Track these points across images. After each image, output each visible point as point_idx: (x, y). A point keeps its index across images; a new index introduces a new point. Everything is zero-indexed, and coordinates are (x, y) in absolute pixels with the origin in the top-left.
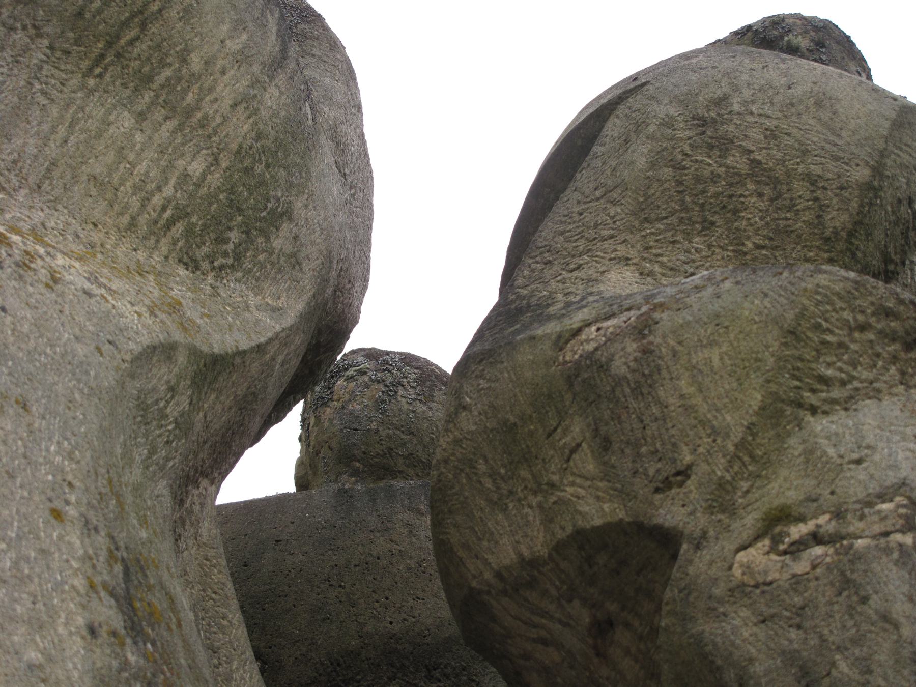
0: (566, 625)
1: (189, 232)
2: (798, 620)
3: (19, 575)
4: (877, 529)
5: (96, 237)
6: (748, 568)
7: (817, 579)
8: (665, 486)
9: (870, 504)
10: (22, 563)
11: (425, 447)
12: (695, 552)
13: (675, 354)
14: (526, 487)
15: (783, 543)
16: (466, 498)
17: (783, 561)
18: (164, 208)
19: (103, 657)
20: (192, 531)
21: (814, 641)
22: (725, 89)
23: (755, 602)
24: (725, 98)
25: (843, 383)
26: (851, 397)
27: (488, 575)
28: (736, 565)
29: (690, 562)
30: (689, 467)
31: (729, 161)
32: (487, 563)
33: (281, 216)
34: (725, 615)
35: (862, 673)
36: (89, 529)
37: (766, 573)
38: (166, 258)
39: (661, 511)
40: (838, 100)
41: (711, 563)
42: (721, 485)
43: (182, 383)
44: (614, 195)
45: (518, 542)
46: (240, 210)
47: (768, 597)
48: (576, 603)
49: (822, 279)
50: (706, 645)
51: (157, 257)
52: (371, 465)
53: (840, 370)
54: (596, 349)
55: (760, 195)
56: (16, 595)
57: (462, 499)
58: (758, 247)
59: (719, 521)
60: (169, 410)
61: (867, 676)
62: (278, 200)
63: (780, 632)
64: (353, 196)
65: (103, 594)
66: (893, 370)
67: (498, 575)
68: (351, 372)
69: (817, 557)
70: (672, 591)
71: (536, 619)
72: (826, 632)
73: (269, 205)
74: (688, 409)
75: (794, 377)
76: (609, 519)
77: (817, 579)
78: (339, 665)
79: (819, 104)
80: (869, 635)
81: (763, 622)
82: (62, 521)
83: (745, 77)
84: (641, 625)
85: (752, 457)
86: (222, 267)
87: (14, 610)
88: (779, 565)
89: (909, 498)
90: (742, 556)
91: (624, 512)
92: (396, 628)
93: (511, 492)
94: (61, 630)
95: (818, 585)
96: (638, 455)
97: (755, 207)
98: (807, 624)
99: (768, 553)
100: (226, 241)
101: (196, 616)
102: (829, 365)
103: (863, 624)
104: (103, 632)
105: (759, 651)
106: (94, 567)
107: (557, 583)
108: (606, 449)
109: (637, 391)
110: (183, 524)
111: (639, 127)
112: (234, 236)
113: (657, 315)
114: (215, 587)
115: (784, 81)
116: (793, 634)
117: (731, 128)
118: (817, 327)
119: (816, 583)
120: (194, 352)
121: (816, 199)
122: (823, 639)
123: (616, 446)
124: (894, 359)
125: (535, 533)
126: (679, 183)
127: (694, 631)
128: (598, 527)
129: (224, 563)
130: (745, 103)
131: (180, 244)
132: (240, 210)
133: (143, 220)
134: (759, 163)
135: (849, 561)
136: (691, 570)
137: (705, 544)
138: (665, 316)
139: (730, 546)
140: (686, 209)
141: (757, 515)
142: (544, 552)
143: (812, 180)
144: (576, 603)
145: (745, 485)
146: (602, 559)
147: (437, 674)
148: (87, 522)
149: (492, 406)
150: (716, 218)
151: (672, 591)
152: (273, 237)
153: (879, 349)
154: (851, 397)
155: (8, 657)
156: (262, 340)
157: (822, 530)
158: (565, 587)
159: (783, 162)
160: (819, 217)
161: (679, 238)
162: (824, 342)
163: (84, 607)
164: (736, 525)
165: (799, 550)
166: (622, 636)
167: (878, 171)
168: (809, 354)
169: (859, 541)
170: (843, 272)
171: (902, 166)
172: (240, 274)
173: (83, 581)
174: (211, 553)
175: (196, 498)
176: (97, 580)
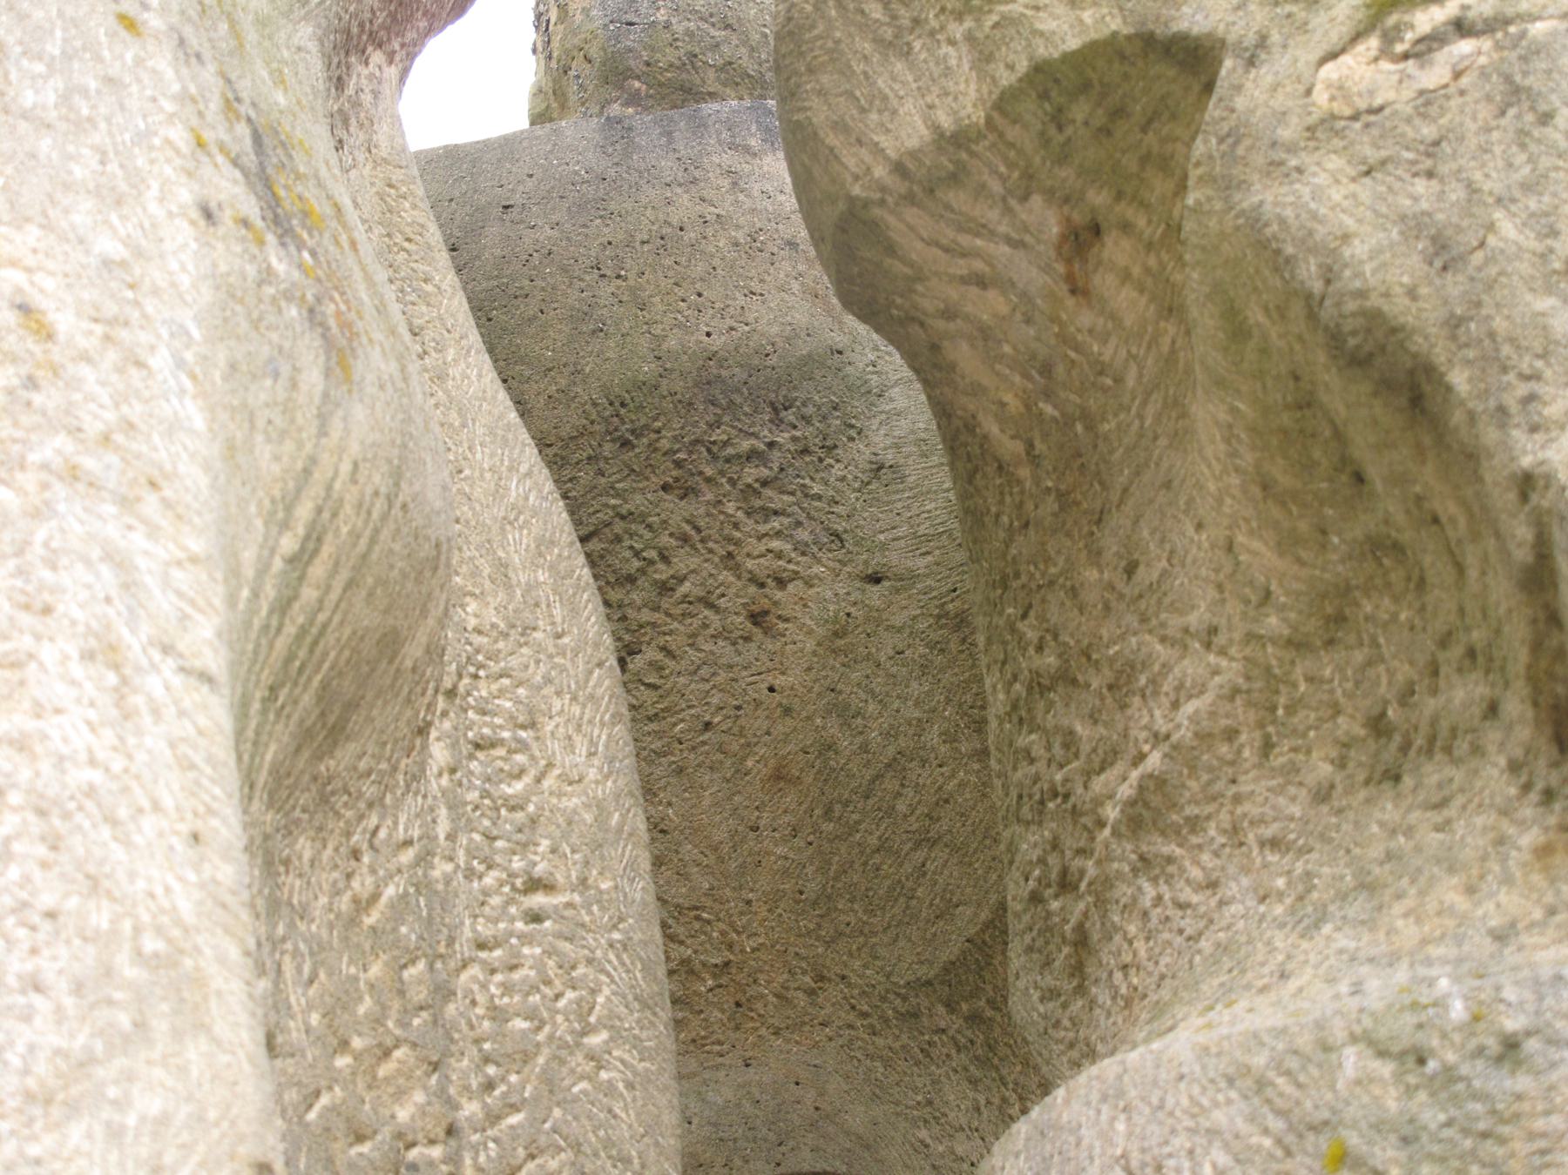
2: (1429, 163)
3: (72, 116)
6: (1340, 90)
7: (1462, 93)
10: (77, 100)
11: (753, 49)
12: (1247, 72)
14: (943, 9)
15: (1402, 40)
16: (838, 42)
17: (1402, 71)
19: (228, 254)
20: (362, 136)
21: (1456, 193)
23: (1352, 143)
27: (880, 171)
28: (1319, 87)
29: (1238, 88)
32: (878, 150)
34: (1299, 170)
35: (1541, 237)
36: (185, 52)
37: (1371, 93)
39: (1185, 9)
41: (1274, 88)
45: (931, 107)
47: (1375, 132)
48: (1037, 201)
50: (1266, 225)
52: (661, 85)
56: (71, 148)
57: (830, 44)
59: (1289, 16)
61: (1549, 242)
63: (1397, 185)
65: (220, 159)
67: (899, 169)
69: (1463, 58)
70: (1206, 142)
71: (965, 240)
72: (1478, 176)
76: (1094, 35)
77: (1462, 93)
78: (623, 405)
80: (1553, 174)
81: (1368, 173)
82: (139, 34)
84: (1150, 222)
87: (70, 173)
88: (1396, 77)
90: (1330, 71)
91: (1119, 20)
92: (717, 342)
94: (153, 207)
95: (1465, 104)
98: (1444, 169)
99: (1376, 59)
103: (1543, 158)
104: (227, 217)
105: (1360, 221)
106: (200, 114)
107: (1002, 169)
110: (346, 122)
114: (408, 230)
116: (1420, 186)
119: (1460, 100)
122: (1472, 189)
125: (962, 87)
127: (1245, 205)
128: (1074, 53)
129: (420, 192)
135: (1521, 58)
136: (1240, 103)
137: (1263, 56)
142: (979, 116)
144: (1037, 201)
146: (1079, 111)
147: (789, 416)
148: (182, 42)
151: (1206, 142)
155: (67, 247)
157: (1471, 14)
158: (1016, 174)
163: (190, 174)
164: (1319, 20)
165: (1430, 50)
166: (1116, 249)
169: (1539, 25)
173: (185, 135)
174: (397, 176)
175: (364, 81)
176: (208, 136)
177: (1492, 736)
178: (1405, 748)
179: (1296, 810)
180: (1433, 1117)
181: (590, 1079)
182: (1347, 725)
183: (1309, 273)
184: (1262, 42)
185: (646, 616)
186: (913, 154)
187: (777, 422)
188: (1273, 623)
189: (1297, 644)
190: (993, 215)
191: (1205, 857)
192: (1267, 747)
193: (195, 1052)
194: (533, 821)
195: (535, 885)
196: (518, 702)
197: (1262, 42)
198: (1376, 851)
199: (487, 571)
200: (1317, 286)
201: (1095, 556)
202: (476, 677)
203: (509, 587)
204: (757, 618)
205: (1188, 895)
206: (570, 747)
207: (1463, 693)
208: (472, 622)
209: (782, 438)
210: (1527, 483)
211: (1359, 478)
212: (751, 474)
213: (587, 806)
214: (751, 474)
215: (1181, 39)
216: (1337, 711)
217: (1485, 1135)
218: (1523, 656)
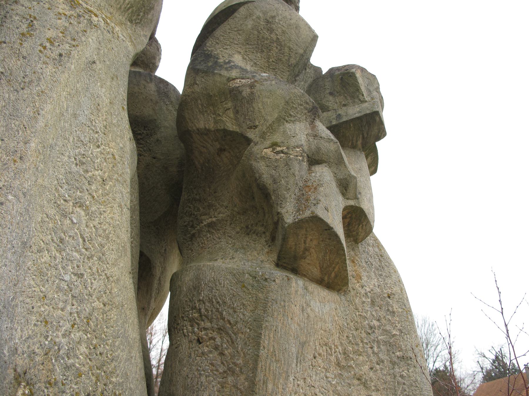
1: (132, 12)
4: (295, 154)
5: (112, 10)
6: (266, 153)
8: (250, 128)
9: (294, 148)
18: (128, 4)
25: (294, 117)
27: (194, 128)
30: (257, 126)
42: (264, 132)
44: (240, 32)
49: (296, 91)
54: (239, 87)
55: (277, 48)
58: (273, 61)
71: (204, 142)
74: (260, 112)
79: (296, 27)
86: (137, 23)
92: (138, 114)
108: (237, 113)
111: (251, 15)
112: (141, 14)
118: (293, 102)
126: (258, 37)
130: (279, 20)
132: (144, 6)
133: (123, 7)
136: (253, 149)
138: (258, 85)
139: (263, 147)
140: (258, 45)
141: (270, 142)
142: (213, 129)
143: (290, 49)
144: (217, 143)
145: (269, 134)
147: (146, 129)
159: (284, 41)
162: (293, 106)
177: (263, 236)
180: (256, 285)
183: (257, 175)
186: (201, 129)
187: (144, 129)
189: (238, 213)
191: (219, 234)
192: (231, 224)
193: (126, 258)
198: (245, 244)
200: (258, 178)
201: (210, 188)
205: (215, 238)
207: (261, 229)
209: (145, 132)
210: (278, 213)
211: (254, 198)
216: (242, 222)
218: (271, 230)
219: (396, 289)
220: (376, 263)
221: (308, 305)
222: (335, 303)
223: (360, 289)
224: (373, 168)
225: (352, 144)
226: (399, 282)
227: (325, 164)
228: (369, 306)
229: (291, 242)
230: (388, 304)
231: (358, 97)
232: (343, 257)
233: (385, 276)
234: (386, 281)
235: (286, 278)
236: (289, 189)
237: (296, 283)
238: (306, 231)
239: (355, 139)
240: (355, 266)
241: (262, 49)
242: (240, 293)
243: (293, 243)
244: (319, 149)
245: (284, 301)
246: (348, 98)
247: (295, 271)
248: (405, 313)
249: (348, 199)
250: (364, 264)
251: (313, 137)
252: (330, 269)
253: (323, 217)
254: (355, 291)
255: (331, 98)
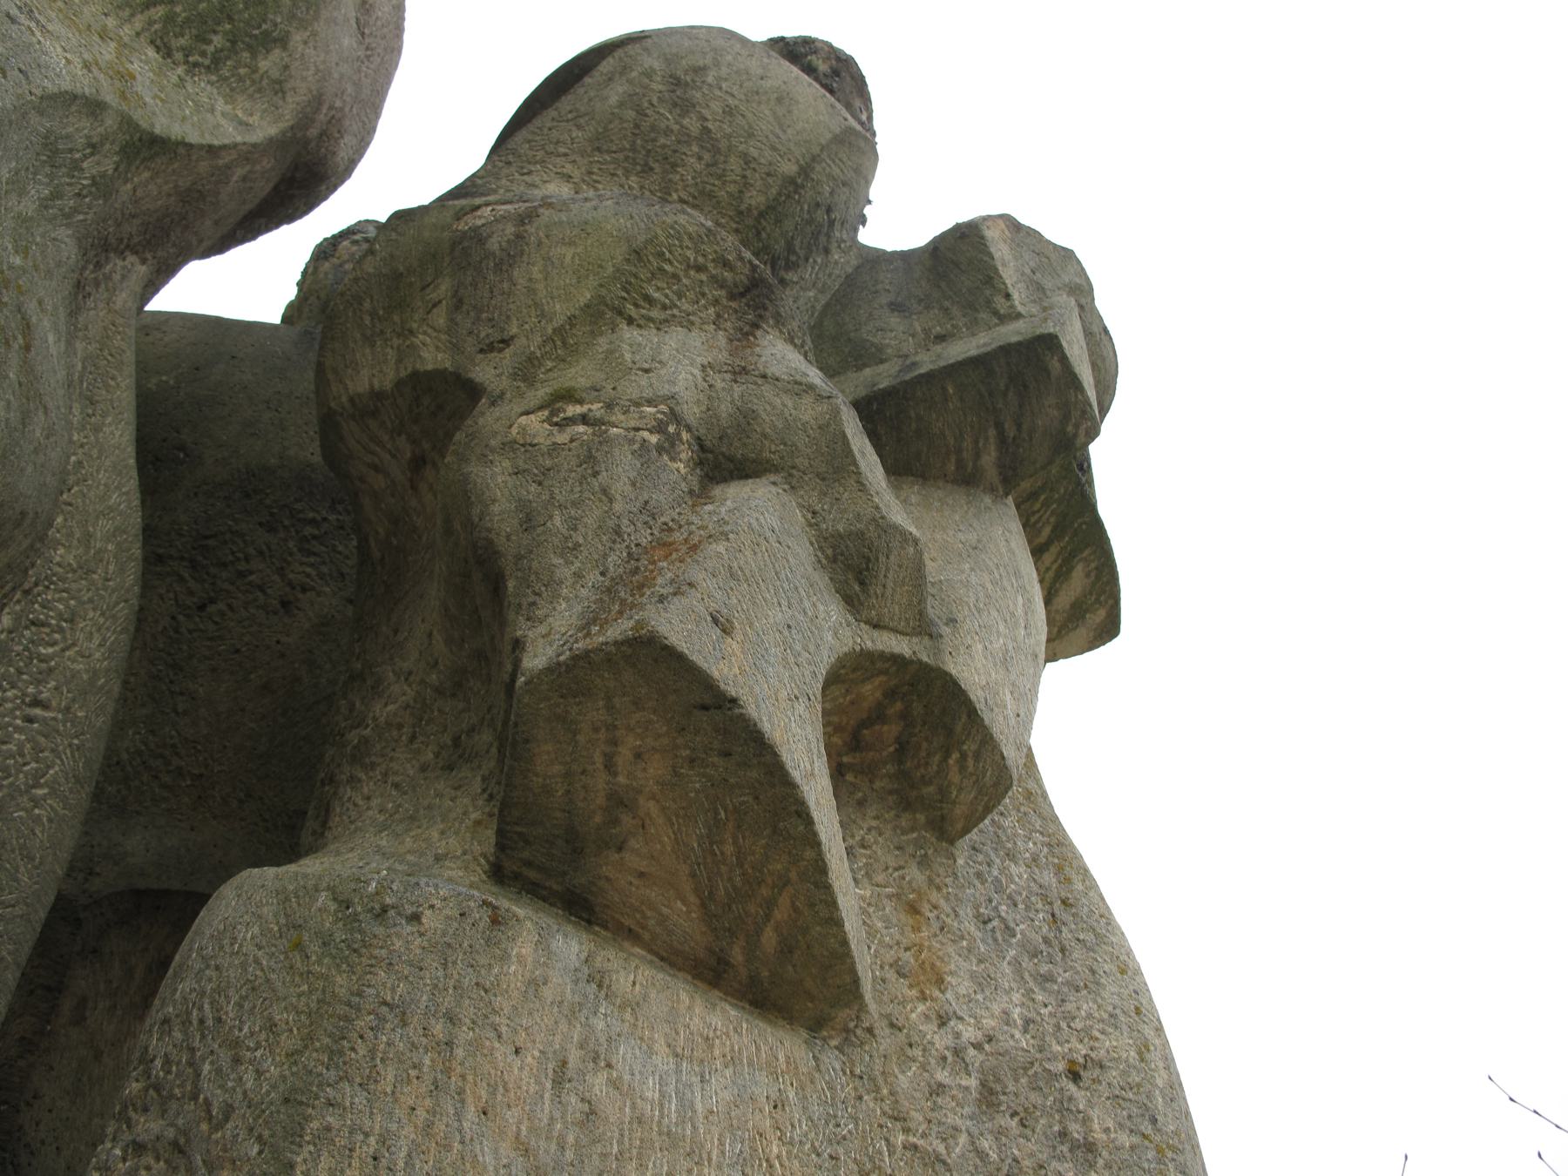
0: (394, 456)
1: (169, 19)
4: (632, 424)
6: (523, 429)
8: (488, 348)
9: (638, 405)
13: (540, 244)
20: (106, 295)
22: (708, 61)
24: (704, 68)
25: (664, 307)
26: (667, 321)
29: (483, 414)
30: (512, 338)
31: (686, 122)
33: (275, 41)
38: (138, 34)
40: (797, 102)
43: (108, 146)
46: (230, 19)
48: (404, 437)
49: (682, 219)
51: (127, 31)
53: (667, 296)
55: (700, 158)
60: (85, 165)
62: (276, 25)
64: (368, 57)
66: (711, 311)
67: (351, 400)
68: (357, 237)
73: (264, 26)
74: (531, 291)
75: (624, 289)
79: (779, 100)
83: (729, 58)
85: (564, 343)
86: (196, 65)
89: (671, 409)
90: (523, 420)
93: (382, 332)
96: (478, 319)
97: (693, 164)
98: (546, 483)
100: (209, 42)
101: (84, 368)
102: (658, 289)
109: (498, 267)
111: (625, 69)
112: (218, 41)
113: (541, 210)
115: (760, 71)
116: (533, 488)
117: (698, 95)
118: (661, 255)
120: (127, 123)
121: (744, 177)
123: (465, 307)
124: (716, 302)
126: (637, 126)
130: (719, 79)
131: (156, 26)
134: (709, 131)
136: (481, 421)
140: (634, 150)
141: (548, 390)
143: (747, 160)
144: (404, 437)
145: (550, 364)
149: (392, 256)
150: (655, 165)
152: (260, 57)
153: (706, 290)
154: (667, 321)
156: (216, 143)
159: (729, 137)
160: (741, 192)
161: (619, 173)
162: (661, 269)
164: (530, 394)
167: (805, 171)
168: (644, 274)
170: (702, 220)
171: (830, 177)
172: (214, 78)
178: (460, 757)
179: (411, 773)
180: (339, 936)
181: (26, 810)
182: (447, 739)
184: (502, 395)
185: (226, 586)
186: (359, 395)
188: (433, 678)
190: (386, 438)
192: (413, 738)
194: (51, 670)
195: (36, 703)
196: (67, 606)
197: (502, 395)
199: (78, 535)
202: (48, 588)
203: (88, 547)
204: (285, 604)
206: (90, 637)
208: (58, 559)
209: (332, 517)
212: (309, 530)
213: (87, 671)
214: (309, 530)
215: (471, 381)
217: (355, 951)
219: (1116, 1044)
220: (1031, 927)
221: (596, 1059)
222: (774, 1075)
223: (929, 1028)
224: (1102, 613)
225: (960, 464)
226: (1138, 1012)
227: (772, 478)
228: (967, 1110)
229: (547, 761)
230: (1064, 1107)
231: (989, 302)
232: (809, 854)
233: (1067, 983)
234: (1070, 1007)
235: (484, 917)
236: (577, 546)
237: (542, 943)
238: (610, 708)
239: (967, 444)
240: (916, 929)
241: (646, 164)
242: (273, 976)
243: (557, 768)
244: (746, 418)
245: (451, 1019)
246: (955, 311)
247: (580, 907)
248: (1151, 1154)
249: (875, 626)
250: (971, 927)
251: (728, 376)
252: (752, 909)
253: (683, 647)
254: (901, 1037)
255: (894, 320)
